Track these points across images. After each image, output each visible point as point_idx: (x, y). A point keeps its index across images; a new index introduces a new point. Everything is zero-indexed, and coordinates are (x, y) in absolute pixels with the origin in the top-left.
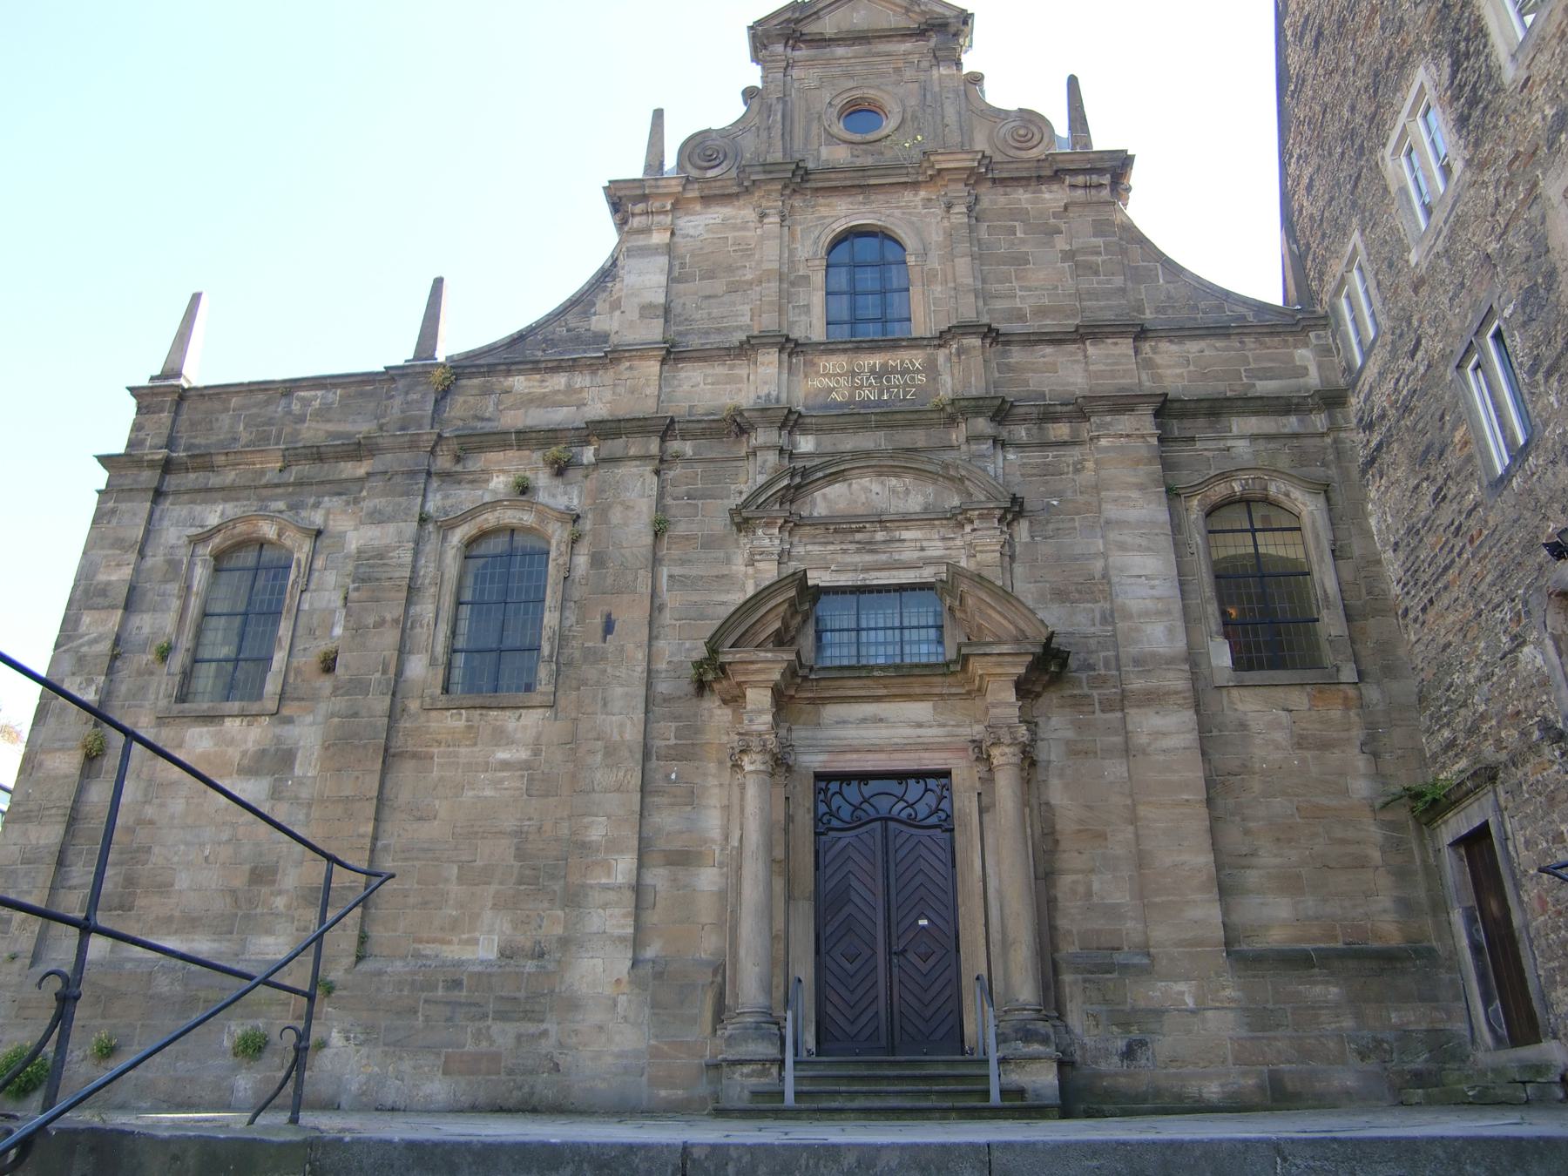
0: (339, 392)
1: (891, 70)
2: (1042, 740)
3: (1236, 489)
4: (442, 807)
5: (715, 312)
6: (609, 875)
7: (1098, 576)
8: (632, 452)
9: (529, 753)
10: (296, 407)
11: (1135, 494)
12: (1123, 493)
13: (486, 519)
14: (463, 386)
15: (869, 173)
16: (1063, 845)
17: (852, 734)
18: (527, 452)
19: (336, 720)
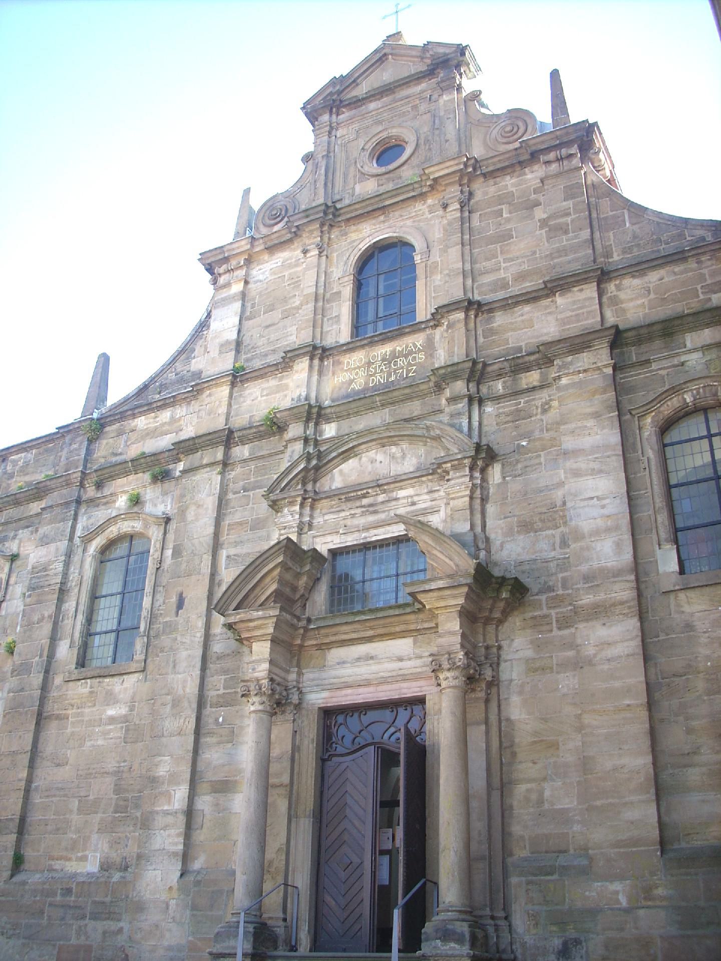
0: (34, 451)
1: (410, 109)
2: (506, 661)
3: (688, 400)
4: (71, 754)
5: (273, 337)
6: (169, 803)
7: (559, 503)
8: (205, 462)
9: (127, 709)
10: (9, 468)
11: (590, 423)
12: (579, 424)
13: (112, 531)
14: (106, 432)
15: (384, 196)
16: (521, 756)
17: (348, 673)
18: (141, 475)
19: (12, 694)
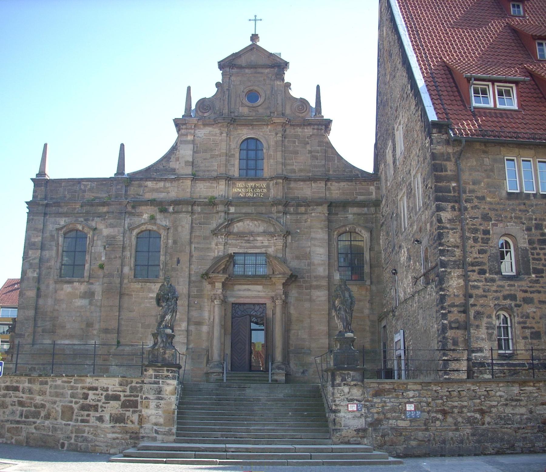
6: (180, 327)
7: (308, 253)
11: (320, 230)
14: (133, 184)
